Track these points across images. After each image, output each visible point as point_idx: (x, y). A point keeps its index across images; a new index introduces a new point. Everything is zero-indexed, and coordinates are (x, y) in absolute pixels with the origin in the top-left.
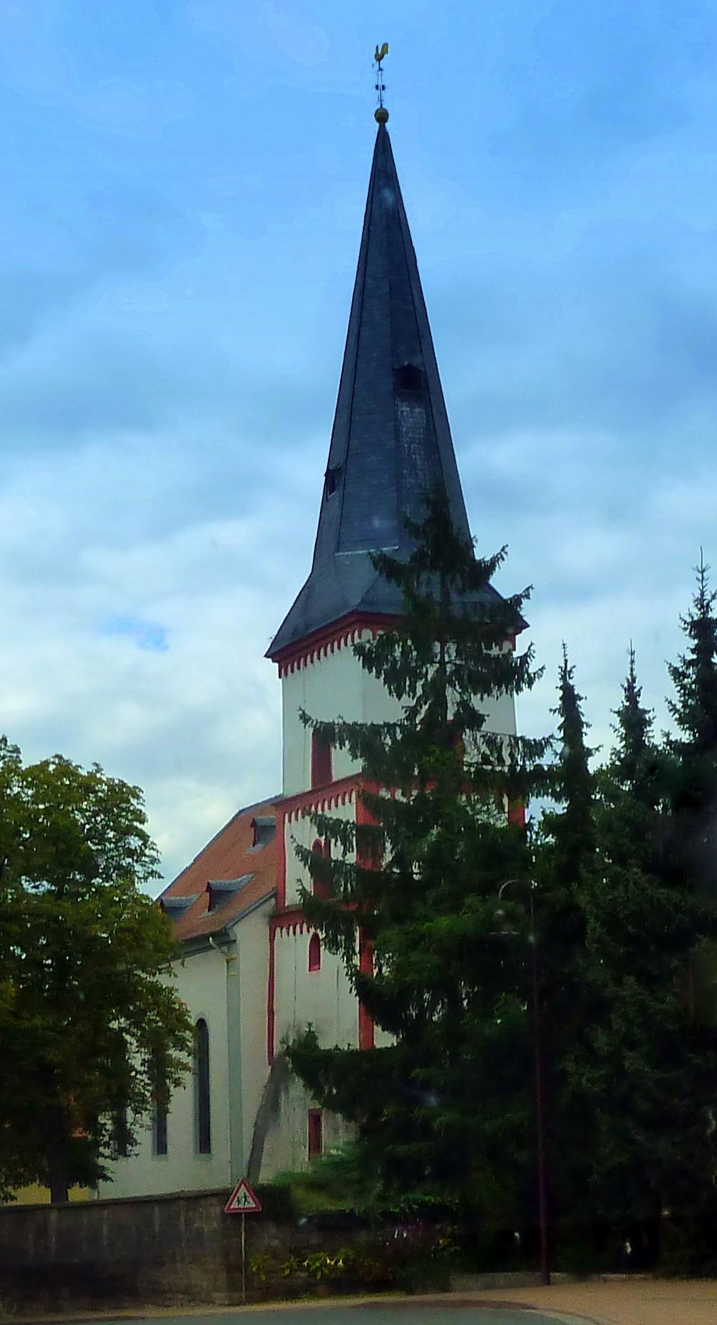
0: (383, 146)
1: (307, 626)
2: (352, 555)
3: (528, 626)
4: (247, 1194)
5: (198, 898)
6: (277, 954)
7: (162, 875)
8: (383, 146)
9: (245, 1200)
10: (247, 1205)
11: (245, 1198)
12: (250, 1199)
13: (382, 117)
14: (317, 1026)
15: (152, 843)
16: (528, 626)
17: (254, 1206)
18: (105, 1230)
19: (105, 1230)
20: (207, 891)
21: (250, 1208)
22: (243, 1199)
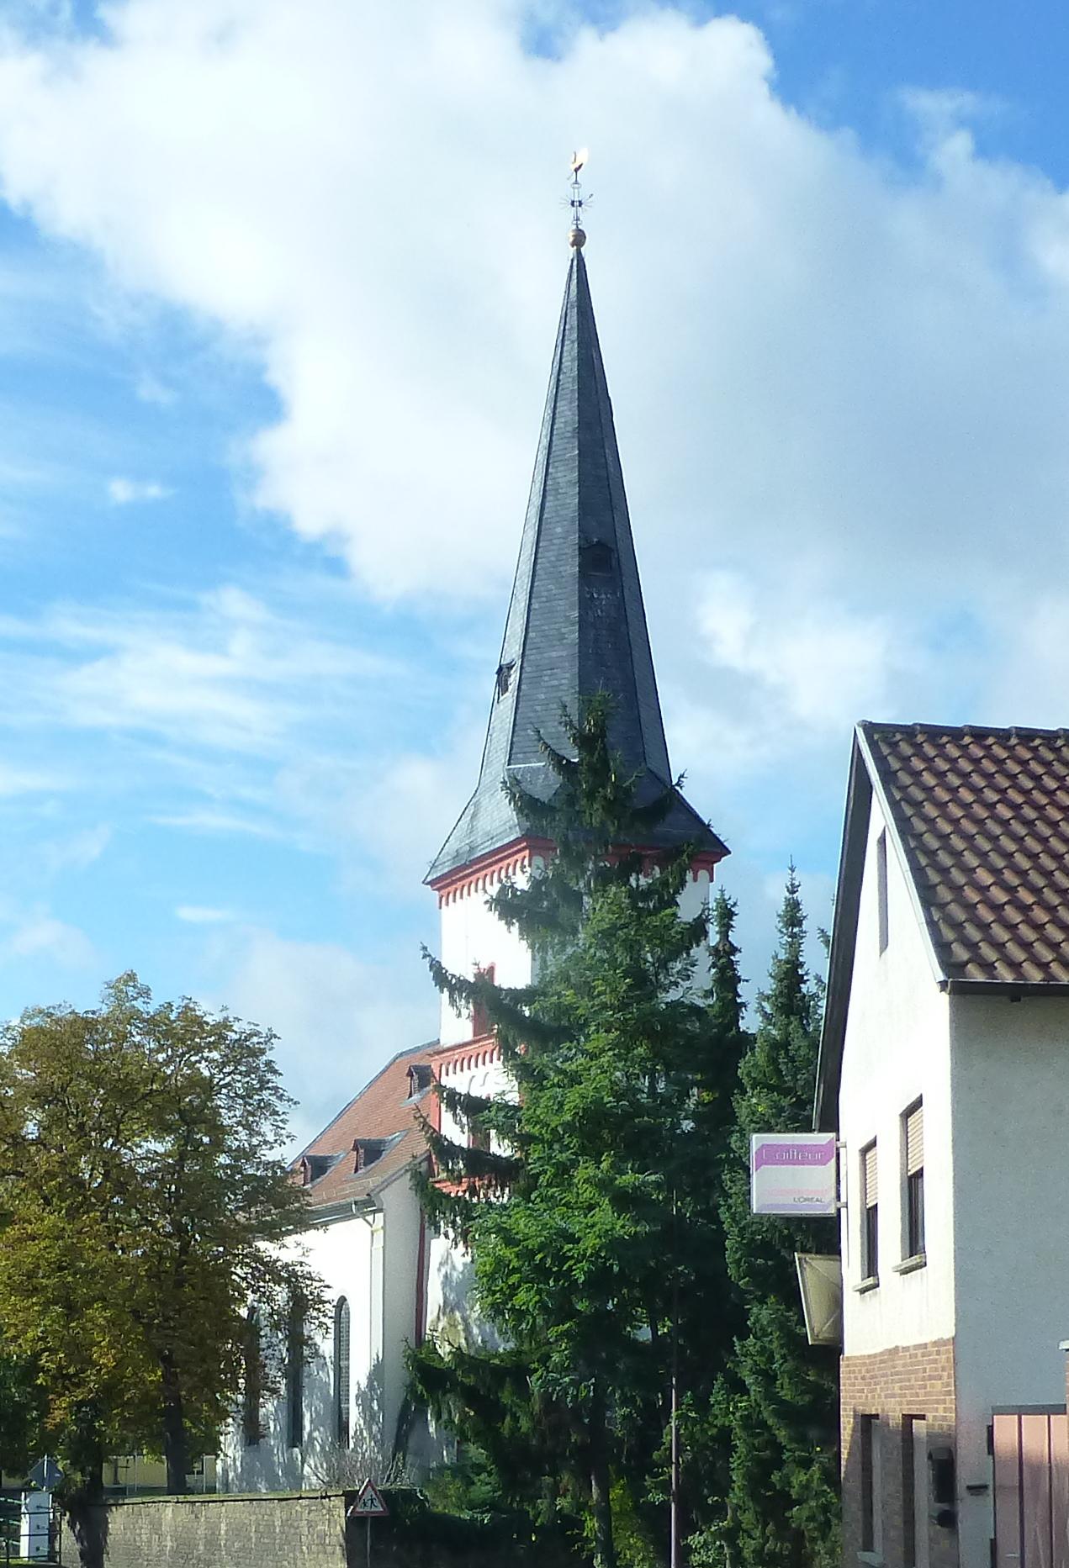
0: (580, 268)
1: (472, 849)
2: (525, 767)
3: (729, 853)
4: (374, 1496)
5: (345, 1158)
6: (998, 1427)
7: (240, 1017)
8: (580, 268)
9: (372, 1502)
10: (374, 1509)
11: (372, 1500)
12: (376, 1502)
13: (579, 239)
14: (75, 1005)
15: (269, 1063)
16: (729, 853)
17: (382, 1510)
18: (223, 1527)
19: (223, 1527)
20: (353, 1150)
21: (377, 1512)
22: (370, 1502)
